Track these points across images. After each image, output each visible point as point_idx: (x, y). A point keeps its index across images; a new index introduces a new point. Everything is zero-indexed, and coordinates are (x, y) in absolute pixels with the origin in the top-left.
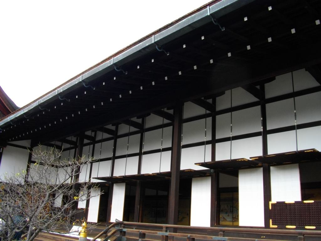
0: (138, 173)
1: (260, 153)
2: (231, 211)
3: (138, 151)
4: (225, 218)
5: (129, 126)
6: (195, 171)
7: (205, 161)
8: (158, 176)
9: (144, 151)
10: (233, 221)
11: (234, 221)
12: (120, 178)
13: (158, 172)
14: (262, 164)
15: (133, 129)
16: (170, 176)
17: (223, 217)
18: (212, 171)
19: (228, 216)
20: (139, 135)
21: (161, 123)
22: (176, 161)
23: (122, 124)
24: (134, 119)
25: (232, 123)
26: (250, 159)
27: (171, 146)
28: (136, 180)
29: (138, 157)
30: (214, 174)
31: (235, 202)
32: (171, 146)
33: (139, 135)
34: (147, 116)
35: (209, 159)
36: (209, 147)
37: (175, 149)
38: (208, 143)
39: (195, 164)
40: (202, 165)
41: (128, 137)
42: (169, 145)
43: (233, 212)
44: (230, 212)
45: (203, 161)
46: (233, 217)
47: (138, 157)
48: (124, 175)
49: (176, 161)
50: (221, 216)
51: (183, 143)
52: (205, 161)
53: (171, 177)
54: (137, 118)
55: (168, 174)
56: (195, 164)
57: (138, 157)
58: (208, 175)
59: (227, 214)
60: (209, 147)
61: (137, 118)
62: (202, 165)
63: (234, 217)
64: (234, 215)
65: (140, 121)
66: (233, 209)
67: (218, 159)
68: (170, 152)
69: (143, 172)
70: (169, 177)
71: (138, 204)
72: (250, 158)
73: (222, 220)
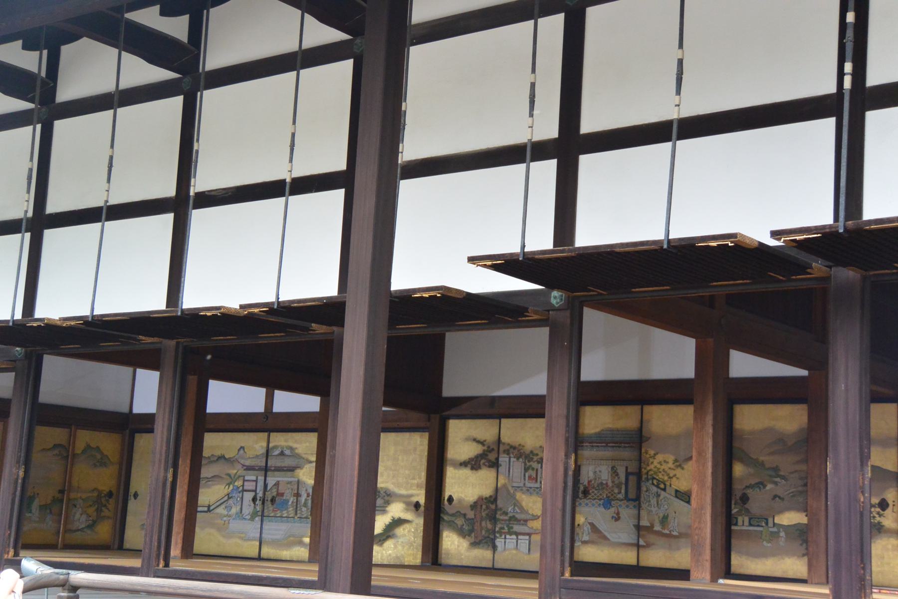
0: (556, 243)
1: (818, 211)
2: (632, 495)
3: (169, 190)
4: (602, 527)
5: (116, 51)
6: (469, 294)
7: (523, 246)
8: (272, 319)
9: (196, 191)
10: (638, 546)
11: (642, 542)
12: (70, 328)
13: (85, 312)
14: (830, 267)
15: (141, 72)
16: (339, 321)
17: (592, 525)
18: (554, 301)
19: (617, 518)
20: (177, 102)
21: (288, 45)
22: (369, 238)
23: (85, 40)
24: (149, 17)
25: (535, 112)
26: (773, 243)
27: (342, 166)
28: (156, 340)
29: (168, 219)
30: (568, 313)
31: (652, 452)
32: (342, 166)
33: (177, 102)
34: (213, 6)
35: (541, 239)
36: (546, 171)
37: (366, 179)
38: (540, 151)
39: (472, 260)
40: (507, 265)
41: (122, 86)
42: (335, 160)
43: (638, 499)
44: (626, 498)
45: (514, 248)
46: (638, 528)
47: (168, 219)
48: (271, 298)
49: (369, 238)
50: (580, 519)
51: (412, 149)
52: (523, 246)
53: (341, 324)
54: (163, 13)
55: (329, 312)
56: (472, 260)
57: (169, 218)
58: (535, 317)
59: (613, 510)
60: (546, 171)
61: (163, 13)
62: (507, 265)
63: (644, 522)
64: (643, 513)
65: (177, 27)
66: (639, 488)
67: (588, 235)
68: (339, 195)
69: (193, 299)
70: (329, 324)
71: (166, 462)
72: (775, 234)
73: (586, 538)
